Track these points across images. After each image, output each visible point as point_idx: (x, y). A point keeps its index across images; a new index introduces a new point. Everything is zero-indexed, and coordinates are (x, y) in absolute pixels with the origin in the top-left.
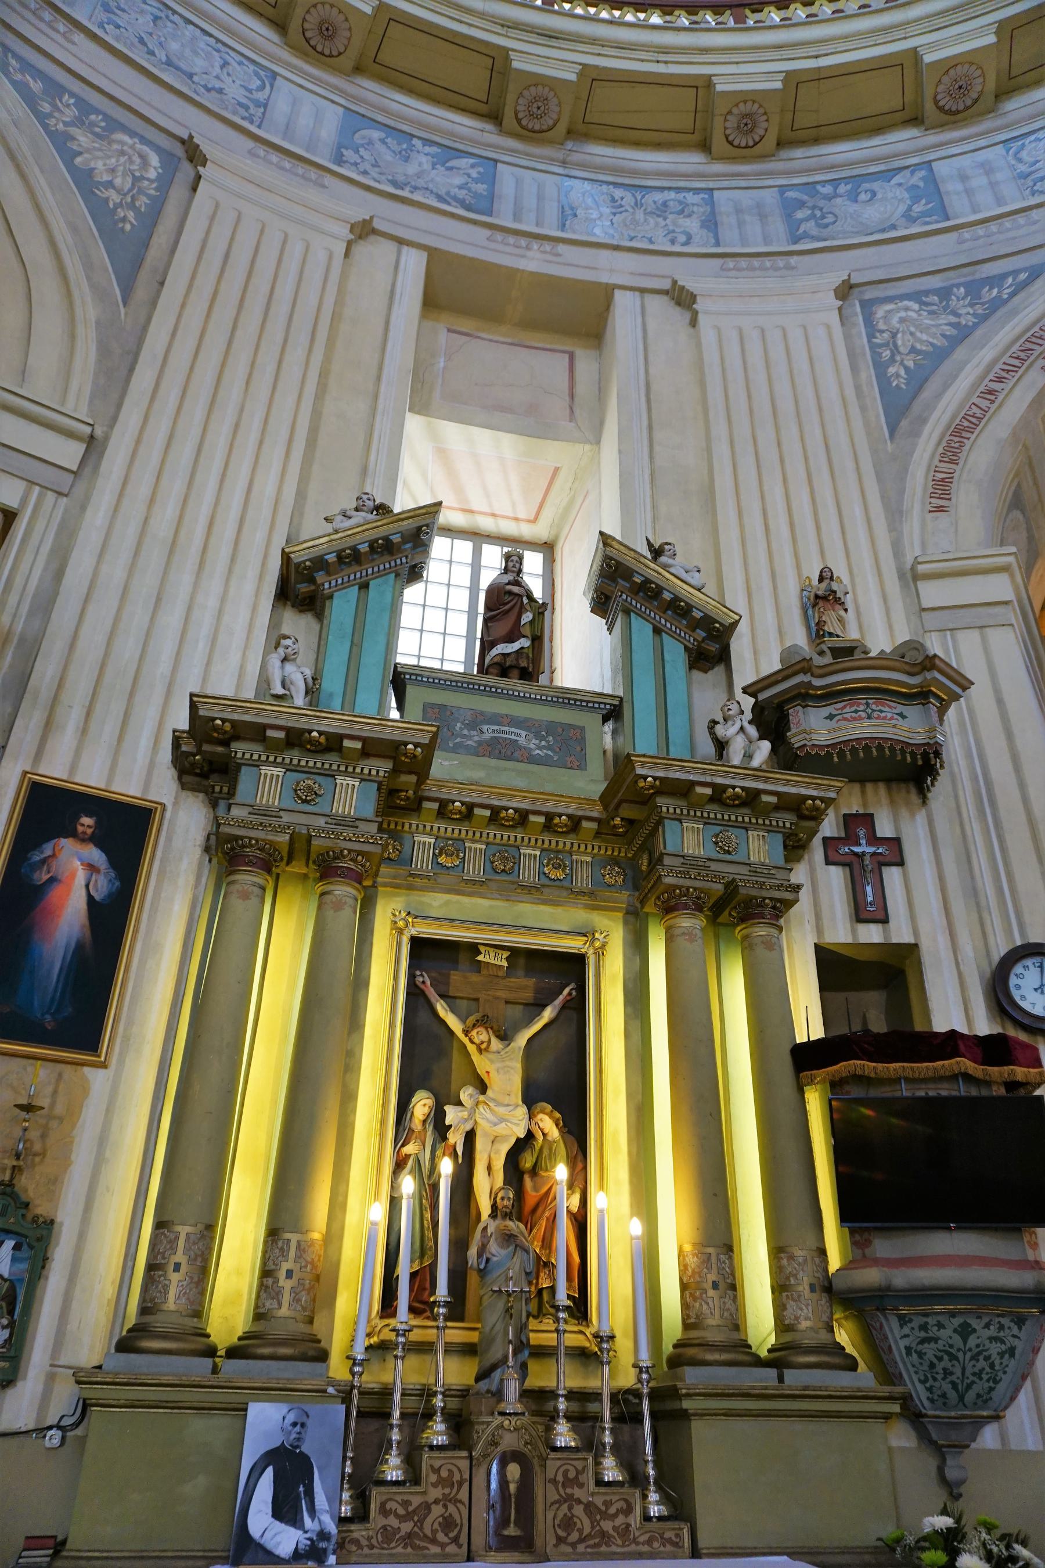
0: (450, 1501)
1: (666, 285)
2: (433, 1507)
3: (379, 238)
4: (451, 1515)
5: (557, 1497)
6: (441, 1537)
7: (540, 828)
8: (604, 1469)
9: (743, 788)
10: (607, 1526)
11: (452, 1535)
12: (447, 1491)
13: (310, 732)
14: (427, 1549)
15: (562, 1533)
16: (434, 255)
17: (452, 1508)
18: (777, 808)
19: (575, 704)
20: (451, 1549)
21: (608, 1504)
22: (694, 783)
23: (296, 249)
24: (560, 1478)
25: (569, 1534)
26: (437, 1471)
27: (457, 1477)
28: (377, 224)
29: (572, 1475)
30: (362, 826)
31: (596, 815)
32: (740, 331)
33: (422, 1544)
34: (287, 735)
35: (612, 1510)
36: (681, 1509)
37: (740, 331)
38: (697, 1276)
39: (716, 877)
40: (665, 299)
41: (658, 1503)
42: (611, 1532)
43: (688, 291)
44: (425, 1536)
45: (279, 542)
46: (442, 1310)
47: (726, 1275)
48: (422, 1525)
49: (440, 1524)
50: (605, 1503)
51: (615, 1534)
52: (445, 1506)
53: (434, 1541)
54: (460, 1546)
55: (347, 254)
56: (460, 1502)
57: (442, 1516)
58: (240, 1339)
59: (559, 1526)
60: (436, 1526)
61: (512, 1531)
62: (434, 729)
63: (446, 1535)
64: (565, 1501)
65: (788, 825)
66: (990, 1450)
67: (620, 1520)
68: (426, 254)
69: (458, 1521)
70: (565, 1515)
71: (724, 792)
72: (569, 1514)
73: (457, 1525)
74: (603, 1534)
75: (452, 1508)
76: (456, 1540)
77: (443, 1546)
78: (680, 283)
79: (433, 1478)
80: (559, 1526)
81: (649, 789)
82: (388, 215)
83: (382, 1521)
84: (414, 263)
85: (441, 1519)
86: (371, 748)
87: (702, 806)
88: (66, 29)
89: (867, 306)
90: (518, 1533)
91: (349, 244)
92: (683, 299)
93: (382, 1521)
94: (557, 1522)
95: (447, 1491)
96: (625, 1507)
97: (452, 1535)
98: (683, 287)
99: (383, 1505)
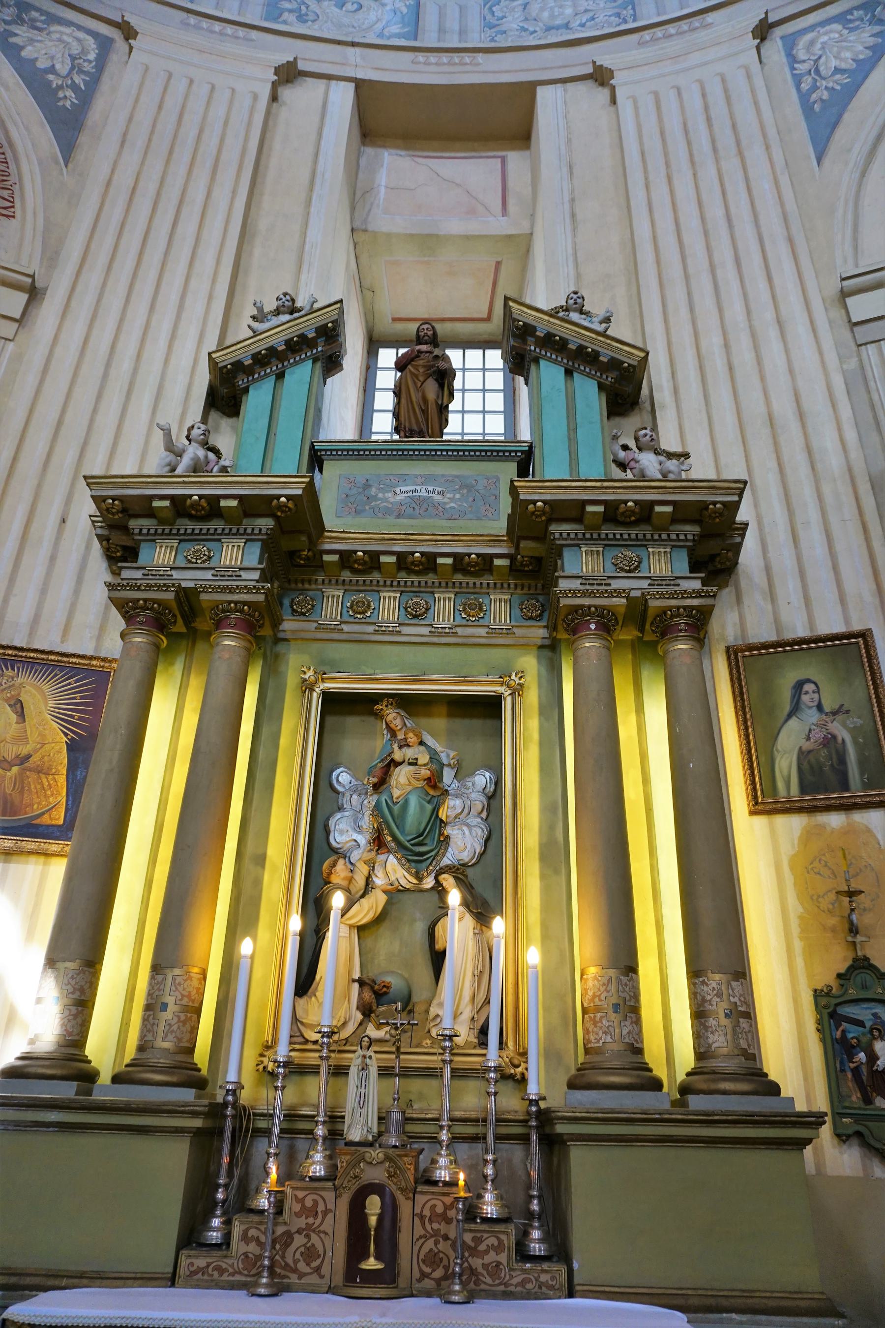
0: (314, 1231)
1: (589, 69)
2: (296, 1236)
3: (307, 79)
4: (313, 1245)
5: (423, 1232)
6: (302, 1266)
7: (450, 569)
8: (484, 1203)
9: (636, 502)
10: (477, 1263)
11: (315, 1264)
12: (311, 1220)
13: (413, 553)
14: (288, 1277)
15: (428, 1270)
16: (360, 85)
17: (314, 1238)
18: (675, 519)
19: (498, 455)
20: (314, 1279)
21: (478, 1241)
22: (585, 503)
23: (179, 87)
24: (426, 1212)
25: (434, 1270)
26: (302, 1201)
27: (321, 1208)
28: (301, 66)
29: (440, 1209)
30: (244, 575)
31: (504, 551)
32: (656, 94)
33: (283, 1273)
34: (398, 559)
35: (483, 1247)
36: (560, 1250)
37: (656, 94)
38: (597, 999)
39: (618, 593)
40: (590, 83)
41: (540, 1241)
42: (480, 1270)
43: (606, 68)
44: (287, 1264)
45: (211, 344)
46: (492, 1075)
47: (628, 998)
48: (284, 1253)
49: (302, 1254)
50: (473, 1239)
51: (485, 1273)
52: (308, 1236)
53: (295, 1271)
54: (322, 1277)
55: (274, 98)
56: (326, 1233)
57: (304, 1245)
58: (127, 1066)
59: (424, 1261)
60: (298, 1255)
61: (371, 1264)
62: (307, 480)
63: (308, 1265)
64: (432, 1236)
65: (690, 537)
66: (848, 1178)
67: (491, 1257)
68: (353, 85)
69: (321, 1252)
70: (431, 1250)
71: (617, 509)
72: (434, 1249)
73: (319, 1256)
74: (473, 1271)
75: (314, 1238)
76: (318, 1270)
77: (301, 1276)
78: (598, 64)
79: (297, 1207)
80: (424, 1261)
81: (540, 516)
82: (311, 57)
83: (243, 1248)
84: (342, 98)
85: (302, 1249)
86: (253, 506)
87: (598, 528)
88: (221, 28)
89: (789, 43)
90: (380, 1266)
91: (275, 85)
92: (601, 76)
93: (243, 1248)
94: (422, 1256)
95: (311, 1220)
96: (496, 1244)
97: (315, 1264)
98: (602, 66)
99: (245, 1232)
